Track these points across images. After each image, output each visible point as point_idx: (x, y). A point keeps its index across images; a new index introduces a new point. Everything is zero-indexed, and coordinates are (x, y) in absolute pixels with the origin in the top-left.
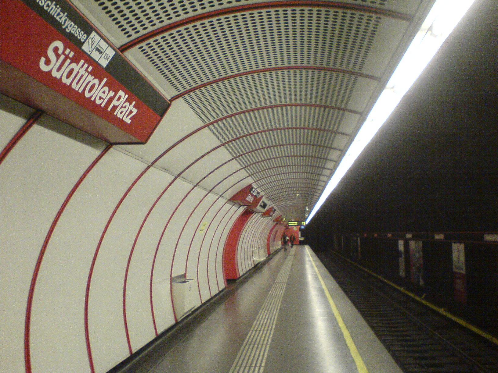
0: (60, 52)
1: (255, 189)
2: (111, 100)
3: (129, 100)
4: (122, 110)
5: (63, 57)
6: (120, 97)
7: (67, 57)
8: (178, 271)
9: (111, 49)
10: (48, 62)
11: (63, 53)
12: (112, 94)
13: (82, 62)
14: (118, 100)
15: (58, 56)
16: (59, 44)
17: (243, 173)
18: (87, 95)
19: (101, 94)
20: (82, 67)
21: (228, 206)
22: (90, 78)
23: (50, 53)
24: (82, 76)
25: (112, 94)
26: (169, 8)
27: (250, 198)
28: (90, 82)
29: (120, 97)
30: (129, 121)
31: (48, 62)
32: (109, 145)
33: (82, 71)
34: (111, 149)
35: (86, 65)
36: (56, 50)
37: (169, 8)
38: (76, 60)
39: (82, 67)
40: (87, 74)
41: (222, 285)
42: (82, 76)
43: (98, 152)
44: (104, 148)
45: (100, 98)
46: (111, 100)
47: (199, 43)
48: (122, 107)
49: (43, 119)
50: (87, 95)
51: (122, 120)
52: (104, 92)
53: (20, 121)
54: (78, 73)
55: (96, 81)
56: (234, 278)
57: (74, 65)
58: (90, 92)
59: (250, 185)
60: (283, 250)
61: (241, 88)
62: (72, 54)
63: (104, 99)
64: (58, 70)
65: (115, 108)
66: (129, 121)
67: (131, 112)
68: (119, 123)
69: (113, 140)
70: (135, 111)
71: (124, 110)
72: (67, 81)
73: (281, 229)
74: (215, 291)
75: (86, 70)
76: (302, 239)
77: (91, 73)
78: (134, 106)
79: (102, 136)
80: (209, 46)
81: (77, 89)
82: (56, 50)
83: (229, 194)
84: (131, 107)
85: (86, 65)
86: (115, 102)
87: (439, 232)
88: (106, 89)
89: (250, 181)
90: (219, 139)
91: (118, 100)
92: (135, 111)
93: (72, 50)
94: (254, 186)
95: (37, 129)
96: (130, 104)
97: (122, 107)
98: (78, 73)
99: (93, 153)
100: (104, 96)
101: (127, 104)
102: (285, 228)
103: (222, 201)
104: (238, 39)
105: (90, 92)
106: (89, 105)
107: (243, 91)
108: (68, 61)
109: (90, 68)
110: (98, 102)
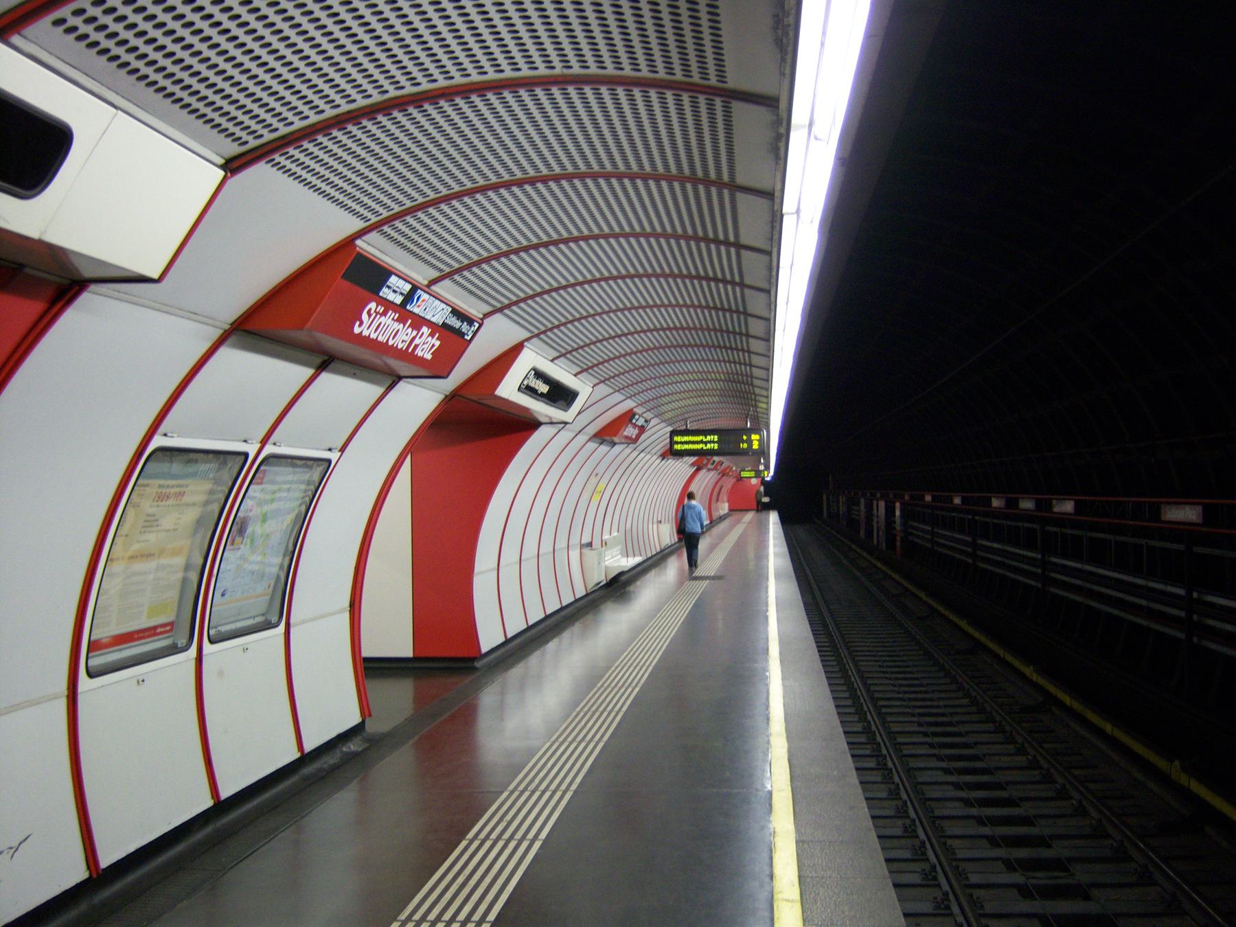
1: (640, 416)
2: (414, 338)
3: (432, 335)
8: (586, 540)
17: (618, 397)
21: (592, 445)
22: (396, 324)
23: (365, 316)
25: (415, 333)
32: (400, 378)
43: (379, 390)
44: (390, 382)
46: (414, 338)
47: (354, 72)
49: (332, 366)
51: (422, 358)
56: (471, 655)
59: (631, 410)
60: (397, 770)
61: (468, 151)
65: (416, 346)
66: (429, 356)
69: (402, 374)
70: (438, 343)
73: (729, 483)
76: (766, 500)
77: (397, 320)
83: (593, 429)
86: (417, 341)
87: (1184, 496)
89: (629, 404)
90: (357, 214)
92: (438, 343)
94: (639, 410)
95: (325, 377)
99: (376, 391)
102: (734, 480)
103: (582, 438)
107: (475, 158)
110: (400, 346)
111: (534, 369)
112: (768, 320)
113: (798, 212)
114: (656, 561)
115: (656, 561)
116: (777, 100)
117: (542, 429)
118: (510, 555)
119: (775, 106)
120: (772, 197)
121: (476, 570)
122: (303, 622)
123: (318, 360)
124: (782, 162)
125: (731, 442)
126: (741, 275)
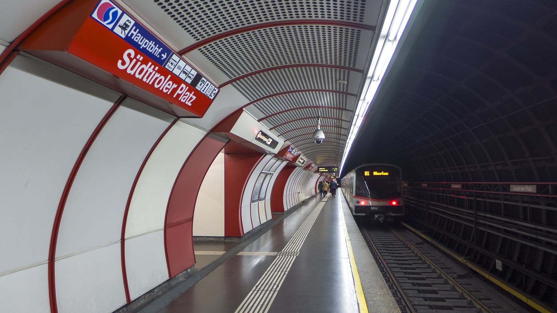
0: (132, 56)
2: (175, 90)
4: (185, 97)
5: (135, 60)
6: (182, 88)
7: (138, 60)
9: (187, 54)
10: (124, 63)
11: (135, 57)
12: (175, 86)
13: (150, 63)
14: (181, 90)
15: (131, 60)
16: (132, 52)
18: (156, 86)
19: (167, 86)
20: (150, 67)
21: (273, 161)
22: (157, 75)
24: (151, 73)
25: (175, 86)
26: (212, 7)
27: (289, 156)
28: (157, 78)
29: (182, 88)
30: (190, 105)
31: (124, 63)
32: (178, 118)
33: (150, 70)
34: (178, 122)
35: (153, 66)
36: (129, 55)
37: (212, 7)
38: (144, 62)
39: (150, 67)
40: (154, 72)
41: (270, 217)
42: (151, 73)
44: (172, 120)
45: (167, 88)
46: (175, 90)
47: (249, 49)
48: (184, 95)
49: (128, 100)
50: (156, 86)
52: (169, 85)
53: (109, 105)
54: (147, 71)
55: (163, 77)
57: (144, 66)
58: (158, 84)
62: (142, 58)
63: (169, 89)
64: (132, 69)
65: (179, 95)
66: (190, 105)
67: (191, 98)
68: (184, 105)
69: (180, 115)
70: (194, 98)
71: (186, 97)
72: (151, 51)
74: (264, 221)
75: (154, 69)
77: (158, 71)
78: (193, 95)
79: (173, 112)
80: (272, 50)
81: (147, 82)
82: (129, 55)
84: (191, 95)
85: (153, 66)
86: (179, 91)
88: (171, 82)
91: (181, 90)
92: (194, 98)
93: (141, 55)
96: (191, 93)
97: (184, 95)
98: (147, 71)
100: (169, 87)
101: (188, 93)
104: (332, 35)
105: (158, 84)
106: (159, 92)
108: (139, 63)
109: (157, 68)
111: (261, 131)
112: (353, 111)
113: (364, 99)
114: (313, 197)
115: (313, 197)
116: (363, 71)
117: (297, 168)
118: (288, 194)
119: (357, 96)
120: (353, 112)
121: (47, 265)
122: (156, 231)
123: (117, 96)
124: (357, 99)
125: (330, 170)
126: (346, 106)
